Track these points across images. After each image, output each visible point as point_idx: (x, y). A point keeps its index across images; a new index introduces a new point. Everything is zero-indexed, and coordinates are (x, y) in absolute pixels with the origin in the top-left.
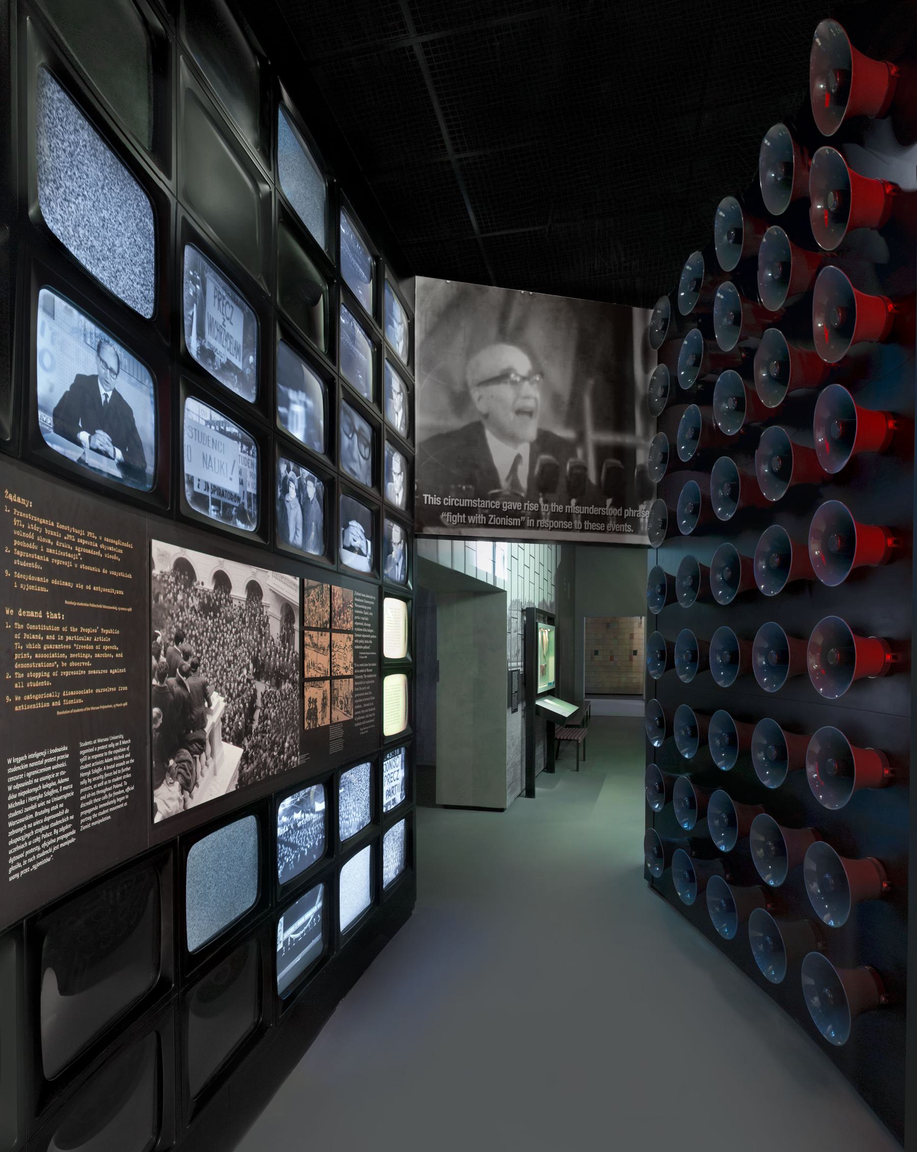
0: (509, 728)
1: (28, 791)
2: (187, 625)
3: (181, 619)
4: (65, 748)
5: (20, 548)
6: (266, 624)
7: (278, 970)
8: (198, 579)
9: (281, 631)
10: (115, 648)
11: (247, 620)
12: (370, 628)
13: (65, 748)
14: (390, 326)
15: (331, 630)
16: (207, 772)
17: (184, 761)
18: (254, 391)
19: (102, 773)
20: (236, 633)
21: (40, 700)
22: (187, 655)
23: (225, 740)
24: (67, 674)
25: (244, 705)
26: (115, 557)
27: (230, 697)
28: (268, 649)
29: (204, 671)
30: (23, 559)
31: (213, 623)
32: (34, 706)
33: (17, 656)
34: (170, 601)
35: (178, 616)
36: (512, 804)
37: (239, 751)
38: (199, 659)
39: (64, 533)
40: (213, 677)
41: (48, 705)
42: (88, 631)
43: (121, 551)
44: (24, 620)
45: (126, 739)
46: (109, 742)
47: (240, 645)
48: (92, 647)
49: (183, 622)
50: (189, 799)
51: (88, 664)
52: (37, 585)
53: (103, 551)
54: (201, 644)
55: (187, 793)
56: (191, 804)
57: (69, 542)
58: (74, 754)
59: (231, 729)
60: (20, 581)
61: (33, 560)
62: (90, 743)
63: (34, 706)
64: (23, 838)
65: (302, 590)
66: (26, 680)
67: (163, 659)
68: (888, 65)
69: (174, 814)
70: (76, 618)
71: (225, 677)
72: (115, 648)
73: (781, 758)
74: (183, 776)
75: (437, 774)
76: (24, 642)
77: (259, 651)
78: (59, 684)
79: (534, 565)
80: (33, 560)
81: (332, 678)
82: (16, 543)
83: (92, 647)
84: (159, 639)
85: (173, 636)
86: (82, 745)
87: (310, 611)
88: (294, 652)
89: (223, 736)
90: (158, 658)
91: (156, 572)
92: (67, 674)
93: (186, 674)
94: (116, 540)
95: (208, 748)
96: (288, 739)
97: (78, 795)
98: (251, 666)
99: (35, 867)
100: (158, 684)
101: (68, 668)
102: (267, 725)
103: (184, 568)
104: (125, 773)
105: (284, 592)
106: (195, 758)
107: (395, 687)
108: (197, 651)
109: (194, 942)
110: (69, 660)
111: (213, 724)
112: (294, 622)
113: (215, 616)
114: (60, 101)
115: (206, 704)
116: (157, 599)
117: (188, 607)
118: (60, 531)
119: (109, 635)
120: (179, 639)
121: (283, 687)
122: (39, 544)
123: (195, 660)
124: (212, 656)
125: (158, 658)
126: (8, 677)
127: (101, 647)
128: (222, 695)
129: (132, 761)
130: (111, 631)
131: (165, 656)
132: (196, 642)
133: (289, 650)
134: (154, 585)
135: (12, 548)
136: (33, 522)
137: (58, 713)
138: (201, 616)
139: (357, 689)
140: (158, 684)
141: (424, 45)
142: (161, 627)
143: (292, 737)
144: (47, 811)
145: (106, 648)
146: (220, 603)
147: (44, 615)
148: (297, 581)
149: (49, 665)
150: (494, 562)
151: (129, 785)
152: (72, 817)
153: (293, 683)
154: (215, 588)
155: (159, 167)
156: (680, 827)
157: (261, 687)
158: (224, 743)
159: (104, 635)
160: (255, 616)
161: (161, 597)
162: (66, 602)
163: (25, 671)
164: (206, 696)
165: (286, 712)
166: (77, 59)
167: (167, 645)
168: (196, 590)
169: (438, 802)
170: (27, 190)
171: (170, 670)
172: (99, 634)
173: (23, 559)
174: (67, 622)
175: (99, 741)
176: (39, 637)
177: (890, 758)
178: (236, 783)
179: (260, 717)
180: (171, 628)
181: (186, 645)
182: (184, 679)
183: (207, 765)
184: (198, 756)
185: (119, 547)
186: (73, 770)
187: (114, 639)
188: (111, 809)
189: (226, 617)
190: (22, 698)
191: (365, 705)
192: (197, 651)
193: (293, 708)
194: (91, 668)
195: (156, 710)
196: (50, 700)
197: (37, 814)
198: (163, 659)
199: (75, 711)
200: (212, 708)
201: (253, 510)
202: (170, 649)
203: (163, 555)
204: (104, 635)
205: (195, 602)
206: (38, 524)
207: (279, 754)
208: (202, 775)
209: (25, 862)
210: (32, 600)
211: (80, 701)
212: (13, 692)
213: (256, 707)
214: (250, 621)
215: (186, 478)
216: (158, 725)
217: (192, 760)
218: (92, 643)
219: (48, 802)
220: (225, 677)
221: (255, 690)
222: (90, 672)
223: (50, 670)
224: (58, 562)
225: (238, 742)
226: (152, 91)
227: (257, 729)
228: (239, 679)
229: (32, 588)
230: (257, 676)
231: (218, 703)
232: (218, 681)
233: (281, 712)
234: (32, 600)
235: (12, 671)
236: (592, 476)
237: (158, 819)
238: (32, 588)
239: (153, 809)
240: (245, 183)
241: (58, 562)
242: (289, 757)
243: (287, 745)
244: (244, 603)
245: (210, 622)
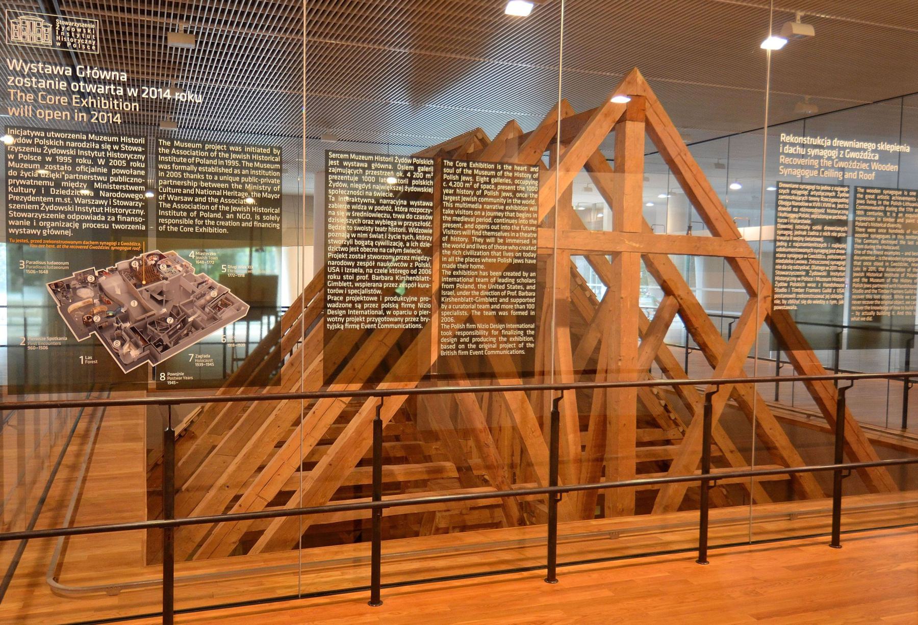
0: (674, 131)
7: (336, 380)
13: (68, 263)
36: (688, 277)
45: (94, 359)
58: (782, 164)
68: (796, 315)
75: (279, 295)
127: (106, 218)
169: (574, 390)
170: (911, 489)
175: (357, 327)
186: (837, 512)
190: (529, 313)
191: (63, 216)
197: (175, 205)
201: (700, 492)
209: (98, 147)
211: (606, 593)
215: (229, 251)
240: (229, 409)
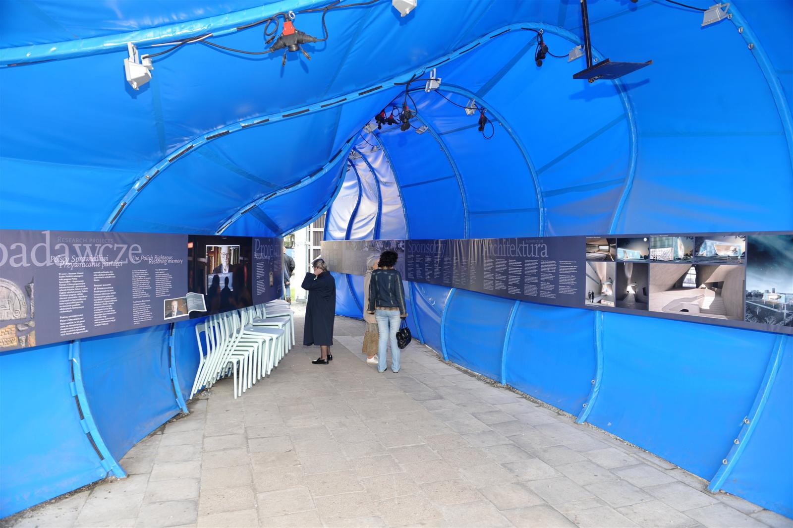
4: (83, 273)
12: (113, 309)
14: (735, 236)
18: (612, 234)
37: (372, 240)
64: (63, 309)
79: (414, 341)
81: (494, 280)
86: (94, 273)
109: (594, 64)
129: (84, 321)
137: (206, 294)
139: (424, 87)
141: (314, 250)
150: (504, 118)
152: (84, 321)
155: (715, 485)
166: (164, 166)
169: (482, 98)
173: (82, 328)
177: (481, 129)
199: (402, 301)
211: (145, 304)
226: (191, 280)
236: (634, 285)
238: (108, 285)
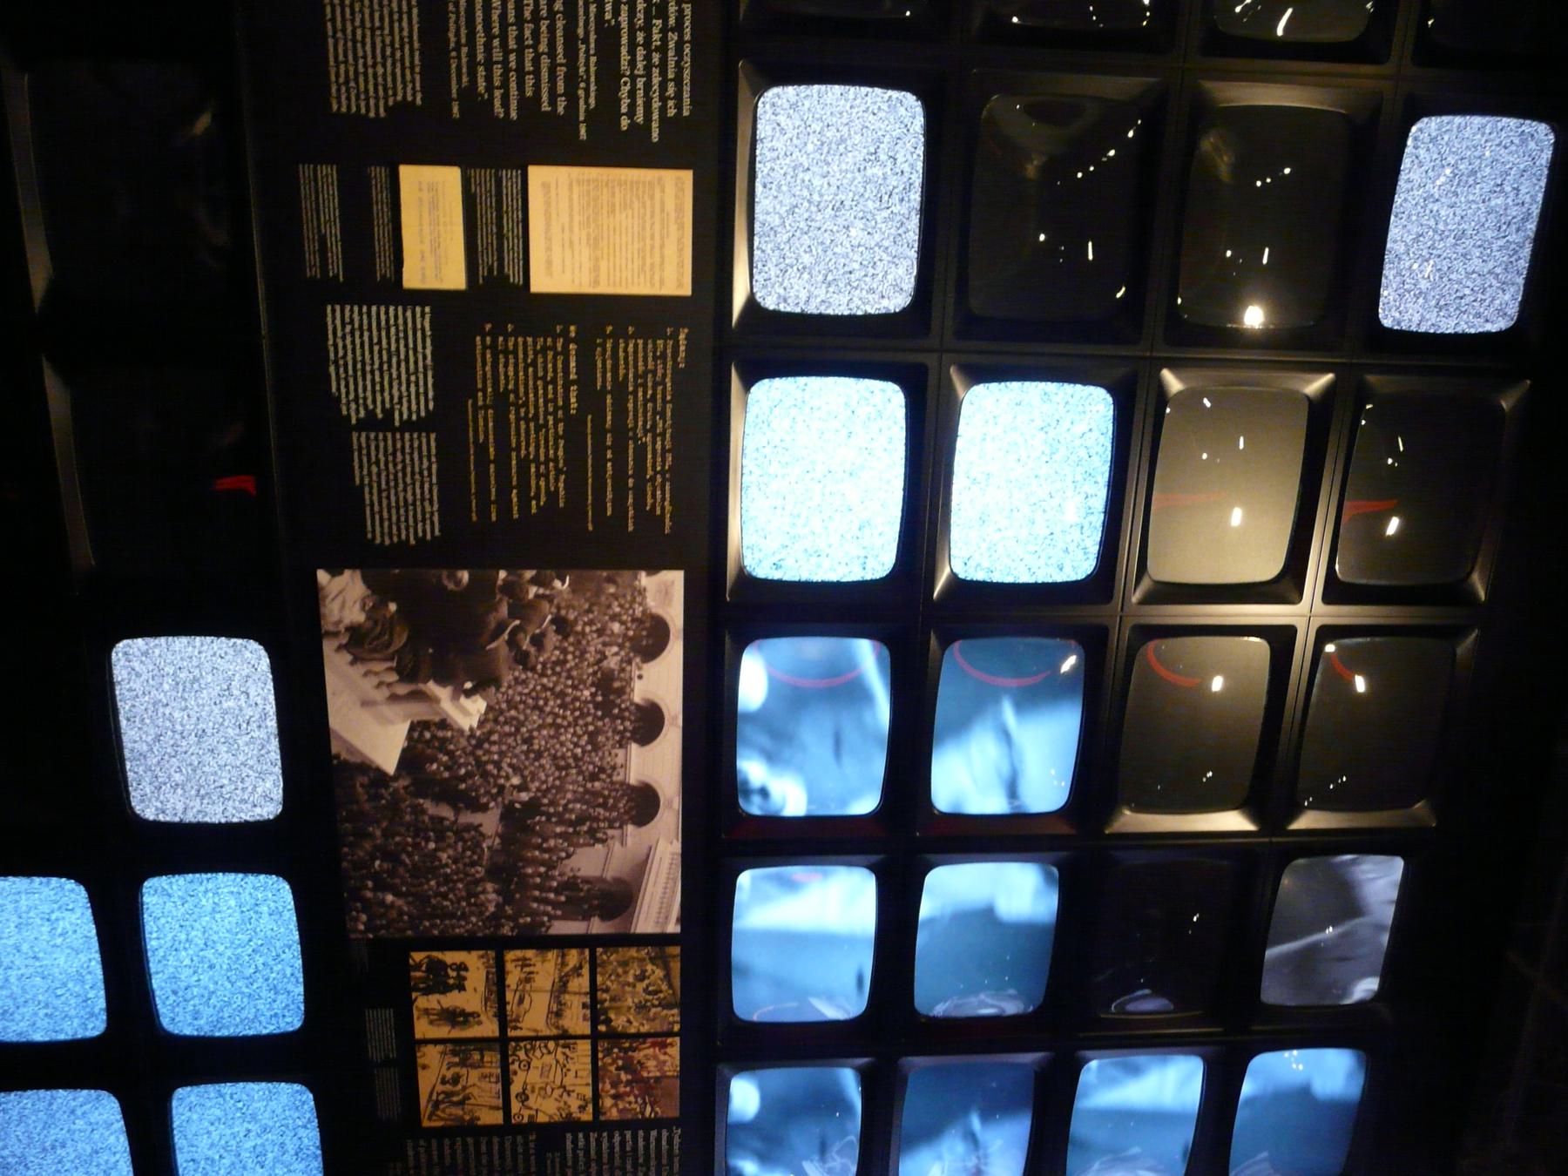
1: (365, 459)
2: (579, 642)
3: (588, 629)
5: (636, 346)
6: (594, 837)
8: (645, 666)
9: (586, 881)
10: (543, 500)
11: (597, 784)
15: (595, 1037)
16: (368, 685)
17: (391, 635)
19: (406, 500)
20: (575, 757)
21: (485, 374)
22: (538, 641)
23: (412, 728)
24: (512, 417)
25: (463, 779)
26: (335, 107)
27: (479, 740)
28: (552, 843)
29: (516, 679)
30: (625, 351)
31: (586, 702)
32: (479, 364)
33: (530, 340)
34: (609, 606)
35: (591, 623)
38: (533, 669)
39: (663, 415)
40: (508, 702)
41: (480, 386)
42: (560, 453)
43: (658, 512)
44: (566, 352)
46: (412, 73)
47: (559, 768)
48: (542, 458)
49: (583, 633)
50: (336, 643)
51: (523, 452)
52: (603, 378)
53: (653, 479)
54: (554, 673)
55: (344, 640)
56: (328, 647)
57: (654, 425)
59: (428, 742)
60: (603, 346)
61: (627, 368)
62: (417, 61)
63: (479, 364)
65: (658, 941)
66: (506, 352)
67: (533, 591)
69: (323, 610)
70: (574, 427)
71: (507, 729)
72: (543, 500)
73: (550, 104)
74: (373, 629)
76: (545, 349)
77: (549, 816)
78: (501, 402)
80: (627, 368)
82: (640, 342)
83: (542, 458)
84: (557, 584)
85: (563, 612)
86: (433, 436)
87: (625, 964)
88: (551, 918)
89: (419, 723)
90: (533, 581)
91: (644, 579)
92: (512, 417)
93: (513, 643)
94: (671, 503)
95: (402, 689)
96: (400, 902)
97: (394, 430)
98: (524, 796)
99: (329, 25)
100: (500, 582)
101: (518, 420)
102: (428, 840)
103: (651, 640)
104: (339, 103)
105: (649, 889)
106: (392, 659)
107: (493, 509)
108: (544, 664)
110: (527, 421)
111: (437, 700)
112: (603, 918)
113: (597, 706)
114: (72, 891)
115: (468, 685)
116: (610, 580)
117: (605, 644)
118: (664, 408)
119: (557, 488)
120: (562, 626)
121: (490, 887)
122: (646, 372)
123: (533, 659)
124: (536, 699)
125: (533, 581)
126: (510, 327)
128: (481, 723)
130: (562, 492)
131: (537, 596)
132: (556, 663)
133: (555, 905)
134: (627, 574)
135: (635, 336)
136: (665, 364)
138: (595, 673)
140: (500, 582)
142: (574, 588)
143: (401, 913)
144: (366, 334)
145: (542, 483)
146: (617, 717)
147: (574, 382)
148: (673, 928)
149: (522, 390)
151: (633, 125)
153: (497, 917)
154: (638, 706)
156: (1330, 641)
157: (490, 822)
158: (407, 725)
159: (557, 480)
160: (604, 805)
161: (612, 590)
162: (609, 513)
163: (515, 352)
164: (485, 681)
165: (445, 896)
167: (550, 599)
168: (629, 662)
171: (522, 609)
172: (558, 472)
174: (568, 419)
176: (550, 375)
178: (344, 756)
179: (442, 819)
180: (574, 608)
181: (553, 639)
182: (506, 636)
183: (380, 684)
184: (394, 664)
185: (663, 508)
187: (553, 496)
188: (367, 489)
189: (598, 731)
192: (544, 664)
193: (453, 916)
194: (518, 456)
195: (465, 576)
196: (484, 390)
198: (533, 591)
200: (463, 699)
202: (546, 606)
203: (667, 593)
204: (557, 480)
205: (612, 663)
206: (664, 376)
207: (376, 877)
208: (366, 674)
210: (586, 367)
211: (529, 93)
212: (494, 334)
213: (457, 811)
214: (596, 794)
216: (446, 582)
217: (391, 650)
218: (547, 459)
219: (396, 17)
220: (507, 729)
221: (484, 808)
222: (514, 454)
223: (516, 391)
224: (630, 406)
225: (410, 759)
227: (424, 812)
228: (504, 765)
229: (599, 365)
230: (508, 814)
231: (468, 712)
232: (502, 712)
233: (447, 879)
234: (586, 367)
235: (515, 334)
237: (322, 576)
238: (599, 365)
239: (335, 571)
241: (630, 406)
242: (367, 906)
243: (390, 898)
244: (620, 778)
245: (587, 693)
